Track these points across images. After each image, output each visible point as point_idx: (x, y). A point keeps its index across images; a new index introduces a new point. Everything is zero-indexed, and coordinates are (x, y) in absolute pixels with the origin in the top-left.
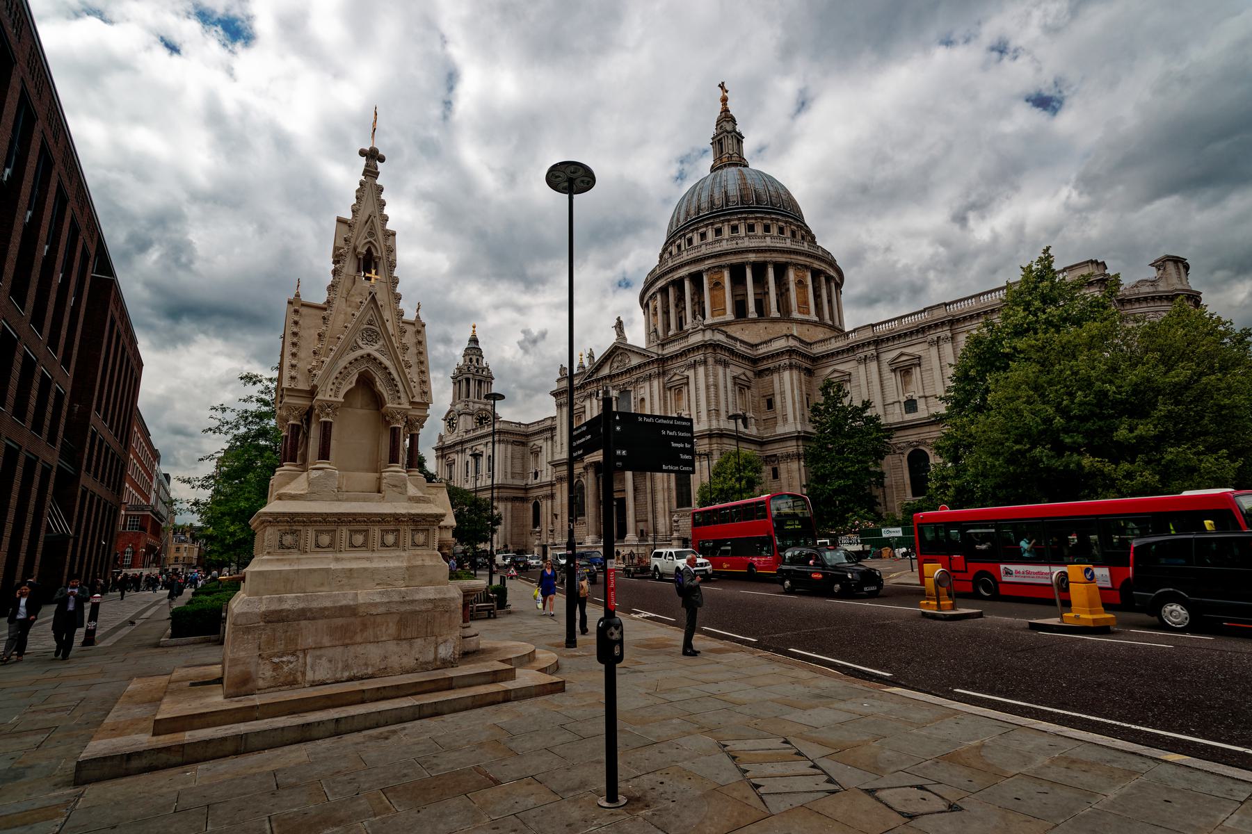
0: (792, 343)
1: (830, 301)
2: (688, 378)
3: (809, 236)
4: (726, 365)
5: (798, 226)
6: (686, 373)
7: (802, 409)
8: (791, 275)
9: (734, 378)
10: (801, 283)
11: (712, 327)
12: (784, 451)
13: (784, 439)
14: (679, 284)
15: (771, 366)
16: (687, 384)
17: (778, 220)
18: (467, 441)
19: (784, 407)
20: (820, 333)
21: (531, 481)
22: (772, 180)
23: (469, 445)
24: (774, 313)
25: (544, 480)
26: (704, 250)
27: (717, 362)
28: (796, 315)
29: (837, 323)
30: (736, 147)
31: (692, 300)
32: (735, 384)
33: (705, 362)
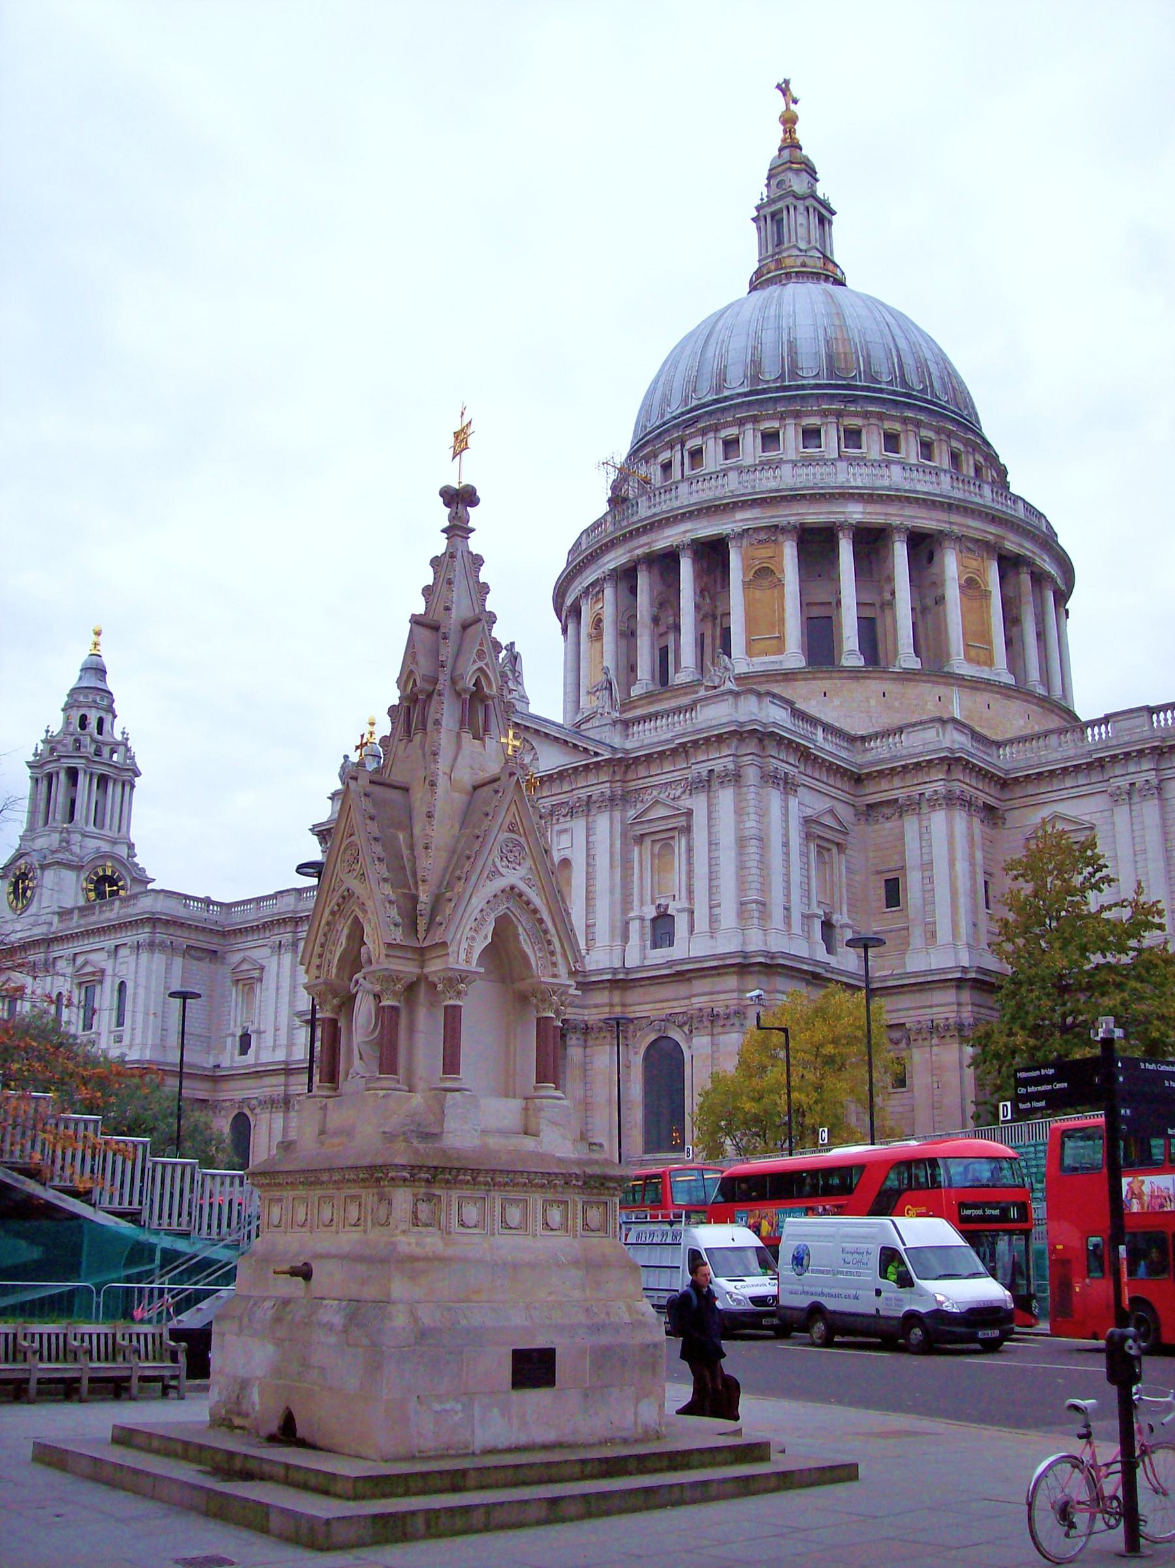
0: (955, 740)
1: (1041, 635)
2: (689, 813)
3: (992, 469)
4: (788, 785)
5: (966, 443)
6: (686, 803)
7: (974, 911)
8: (951, 564)
9: (807, 821)
10: (971, 586)
11: (749, 685)
12: (926, 1015)
13: (924, 985)
14: (667, 561)
15: (900, 794)
16: (688, 830)
17: (918, 424)
19: (928, 900)
20: (1012, 719)
21: (230, 1058)
22: (944, 361)
23: (69, 949)
24: (907, 658)
25: (265, 1057)
26: (733, 485)
27: (771, 779)
28: (959, 665)
29: (1057, 693)
30: (815, 233)
31: (697, 607)
32: (808, 836)
33: (736, 778)
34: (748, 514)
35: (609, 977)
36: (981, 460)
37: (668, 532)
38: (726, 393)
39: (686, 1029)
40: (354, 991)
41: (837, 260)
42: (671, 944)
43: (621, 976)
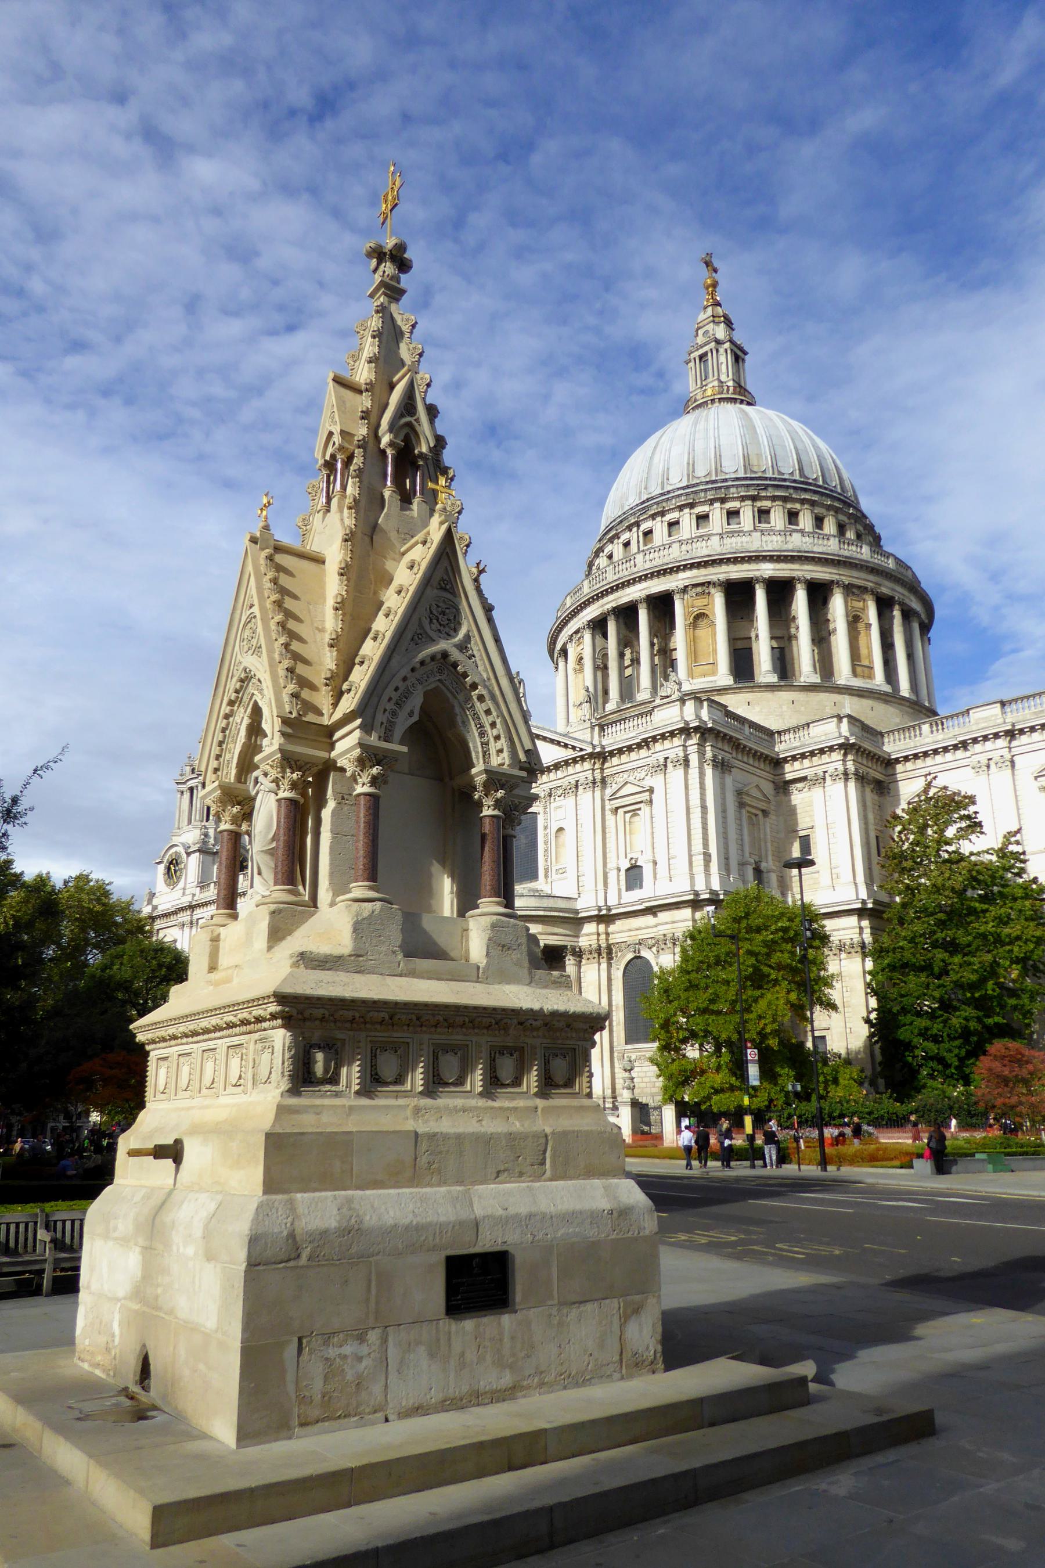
5: (850, 516)
6: (648, 783)
9: (739, 793)
10: (854, 621)
14: (627, 614)
15: (809, 773)
18: (199, 906)
26: (676, 554)
32: (741, 805)
34: (688, 574)
35: (596, 913)
36: (861, 529)
37: (628, 590)
38: (670, 488)
39: (654, 949)
40: (253, 793)
41: (748, 388)
42: (641, 887)
43: (604, 912)
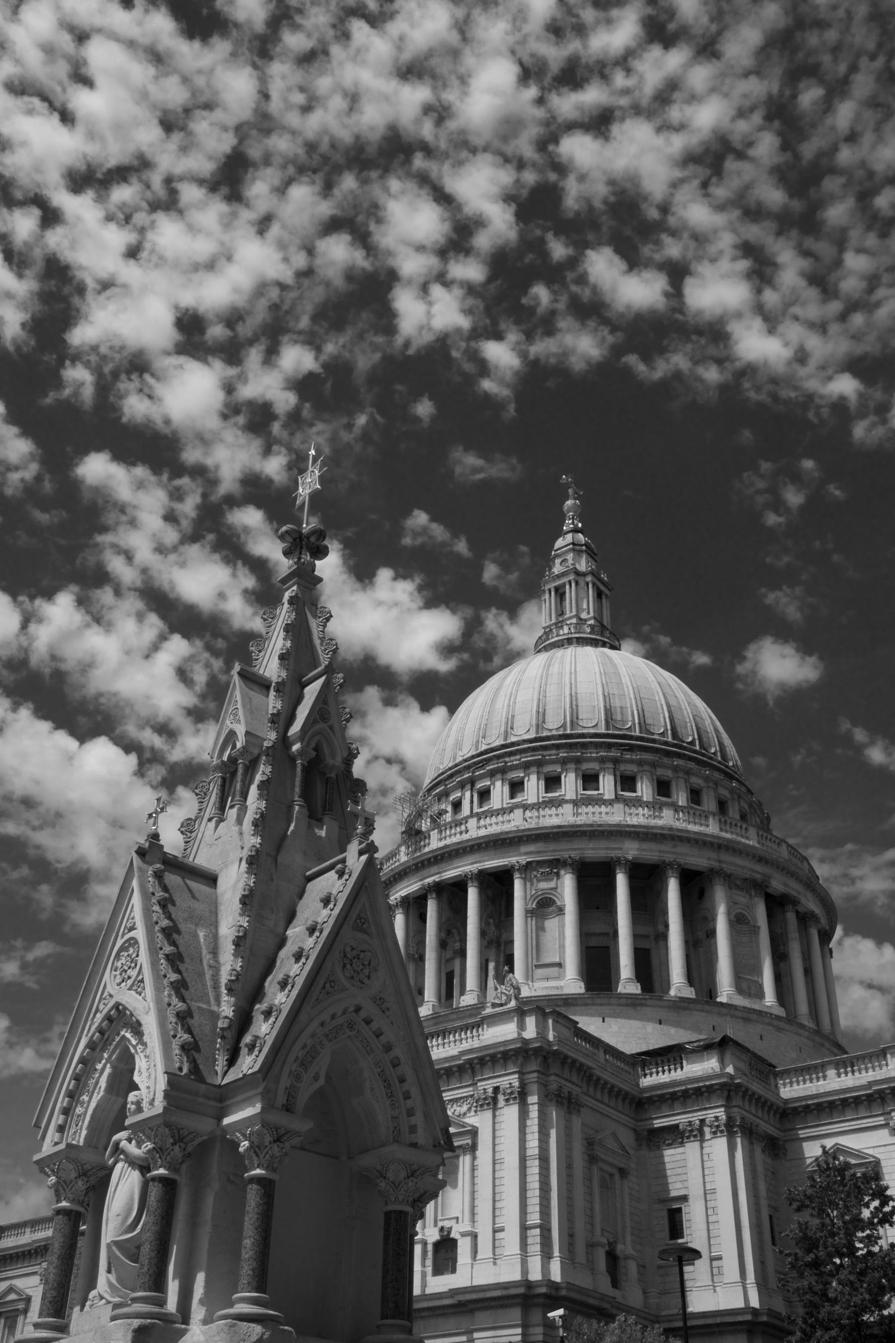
1: (808, 971)
10: (740, 923)
14: (451, 895)
26: (516, 822)
